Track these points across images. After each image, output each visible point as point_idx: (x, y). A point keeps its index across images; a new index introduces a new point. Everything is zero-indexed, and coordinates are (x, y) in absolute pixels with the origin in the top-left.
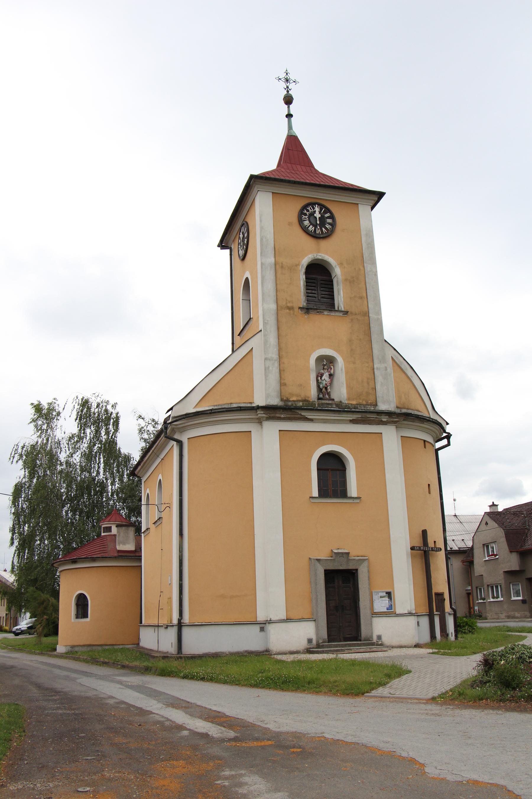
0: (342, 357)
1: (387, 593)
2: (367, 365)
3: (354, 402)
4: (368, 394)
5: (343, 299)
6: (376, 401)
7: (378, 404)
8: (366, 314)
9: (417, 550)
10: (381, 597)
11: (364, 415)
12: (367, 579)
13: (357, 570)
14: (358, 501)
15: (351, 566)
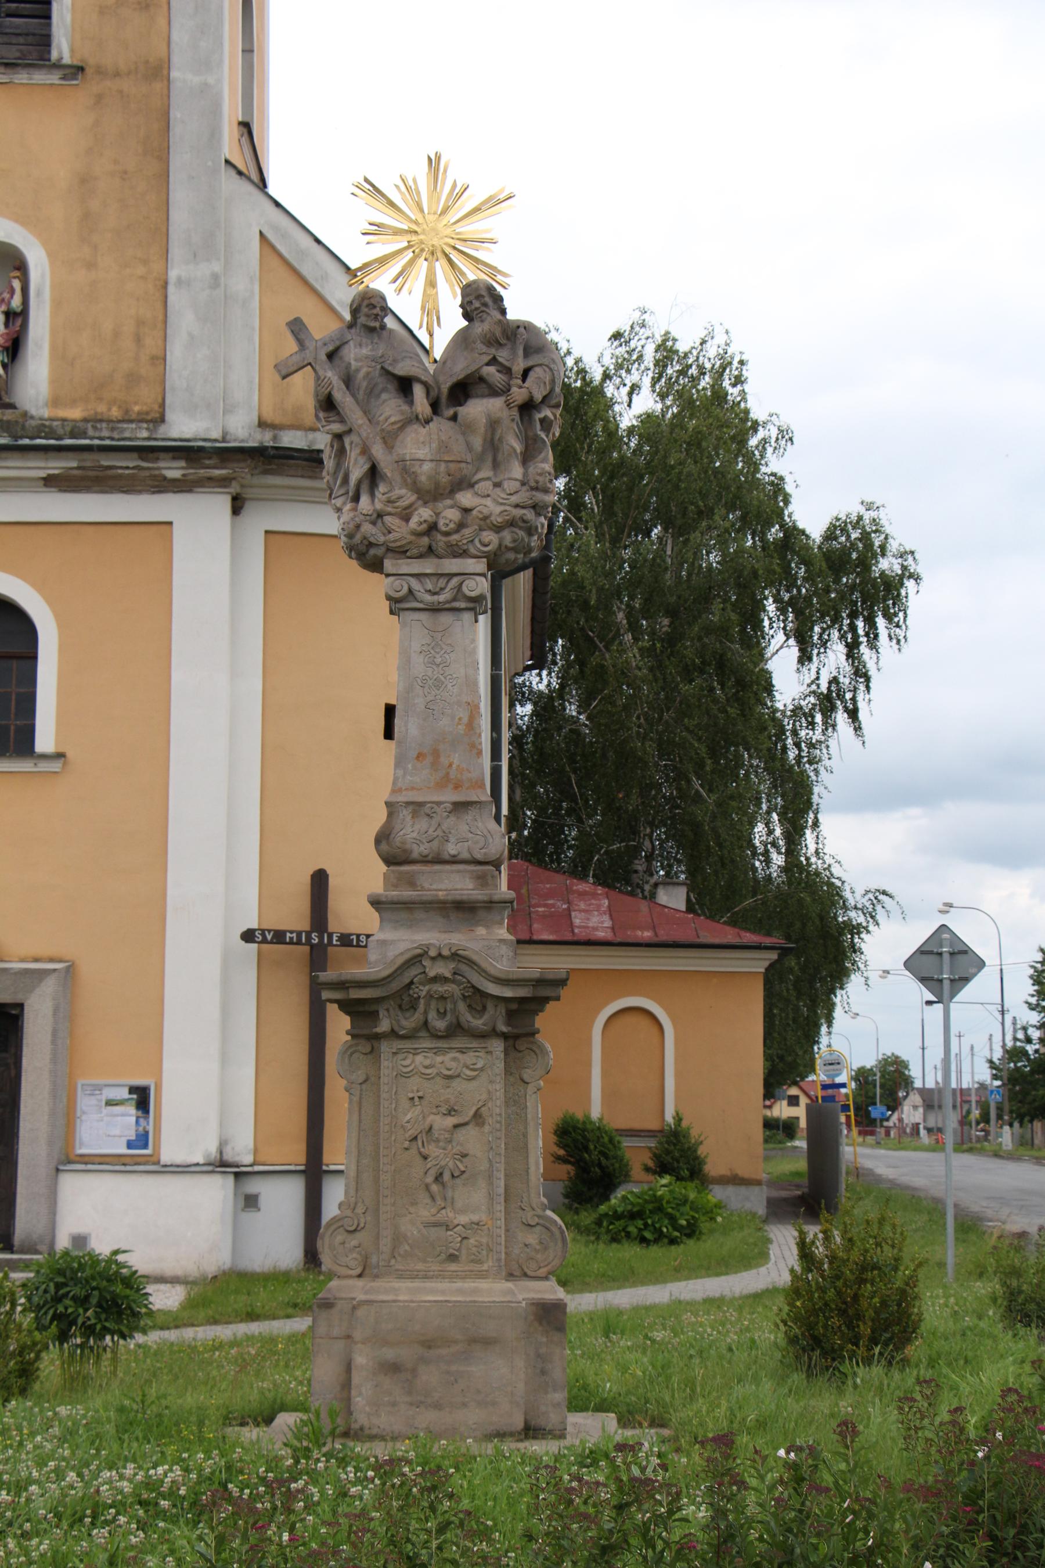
0: (45, 244)
1: (133, 1090)
2: (141, 270)
3: (75, 413)
4: (133, 379)
5: (68, 18)
6: (163, 405)
7: (169, 416)
8: (158, 71)
9: (291, 943)
10: (110, 1103)
11: (89, 459)
12: (49, 1037)
14: (56, 766)
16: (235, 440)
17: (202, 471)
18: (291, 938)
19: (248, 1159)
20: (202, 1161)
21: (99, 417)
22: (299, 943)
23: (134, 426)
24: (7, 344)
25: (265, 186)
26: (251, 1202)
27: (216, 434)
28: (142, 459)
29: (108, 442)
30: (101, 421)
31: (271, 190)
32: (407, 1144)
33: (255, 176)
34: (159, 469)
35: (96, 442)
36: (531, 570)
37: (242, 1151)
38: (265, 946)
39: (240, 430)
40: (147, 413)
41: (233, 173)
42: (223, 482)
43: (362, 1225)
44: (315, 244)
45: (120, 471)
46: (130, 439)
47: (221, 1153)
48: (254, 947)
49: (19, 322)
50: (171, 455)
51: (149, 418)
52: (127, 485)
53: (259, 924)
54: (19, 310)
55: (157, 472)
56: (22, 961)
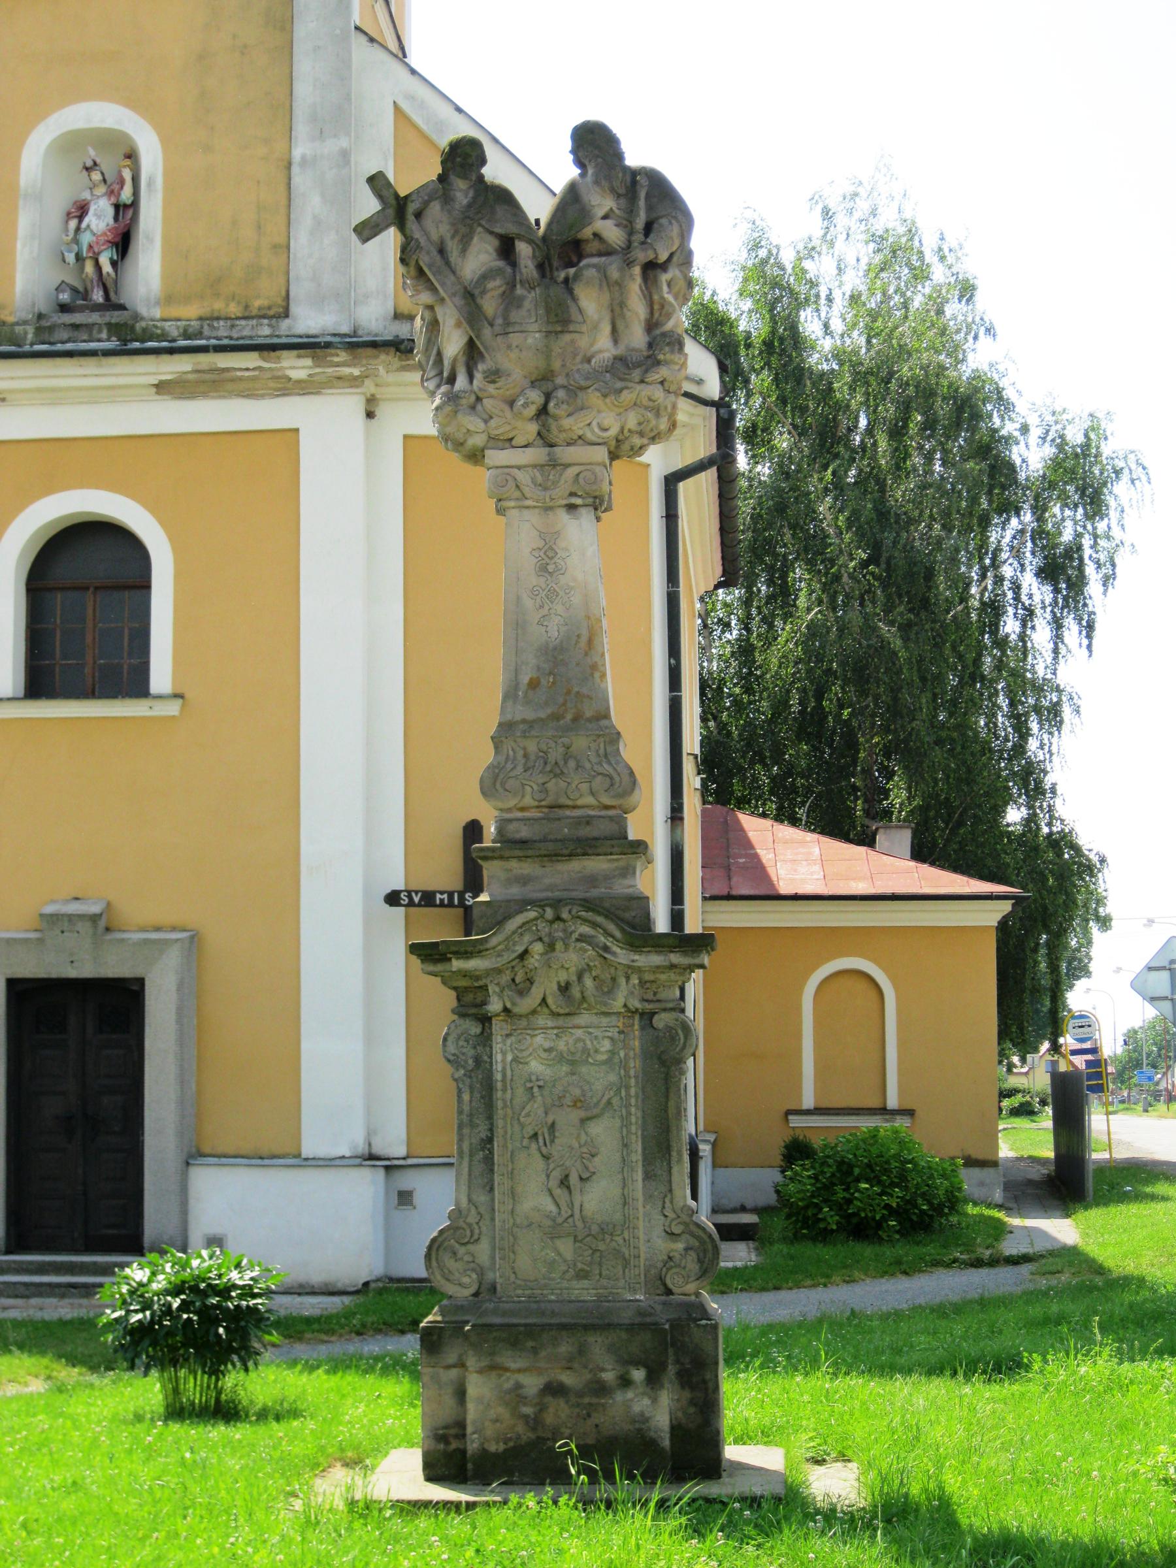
0: (157, 127)
7: (294, 309)
9: (442, 905)
11: (204, 360)
13: (141, 982)
15: (113, 966)
16: (369, 334)
17: (330, 370)
18: (442, 900)
19: (401, 1151)
20: (348, 1154)
21: (216, 315)
22: (451, 904)
23: (254, 322)
24: (117, 240)
25: (405, 56)
26: (405, 1198)
27: (345, 329)
28: (264, 360)
29: (225, 342)
30: (218, 319)
31: (414, 60)
32: (526, 1142)
33: (393, 45)
34: (282, 368)
35: (213, 342)
36: (715, 468)
37: (394, 1143)
38: (412, 909)
39: (373, 322)
40: (269, 308)
41: (363, 39)
42: (355, 382)
43: (476, 1237)
44: (456, 113)
45: (239, 374)
46: (251, 338)
47: (370, 1145)
48: (400, 911)
49: (130, 213)
50: (295, 353)
51: (271, 313)
52: (247, 388)
53: (406, 884)
54: (129, 202)
55: (280, 374)
56: (143, 930)
